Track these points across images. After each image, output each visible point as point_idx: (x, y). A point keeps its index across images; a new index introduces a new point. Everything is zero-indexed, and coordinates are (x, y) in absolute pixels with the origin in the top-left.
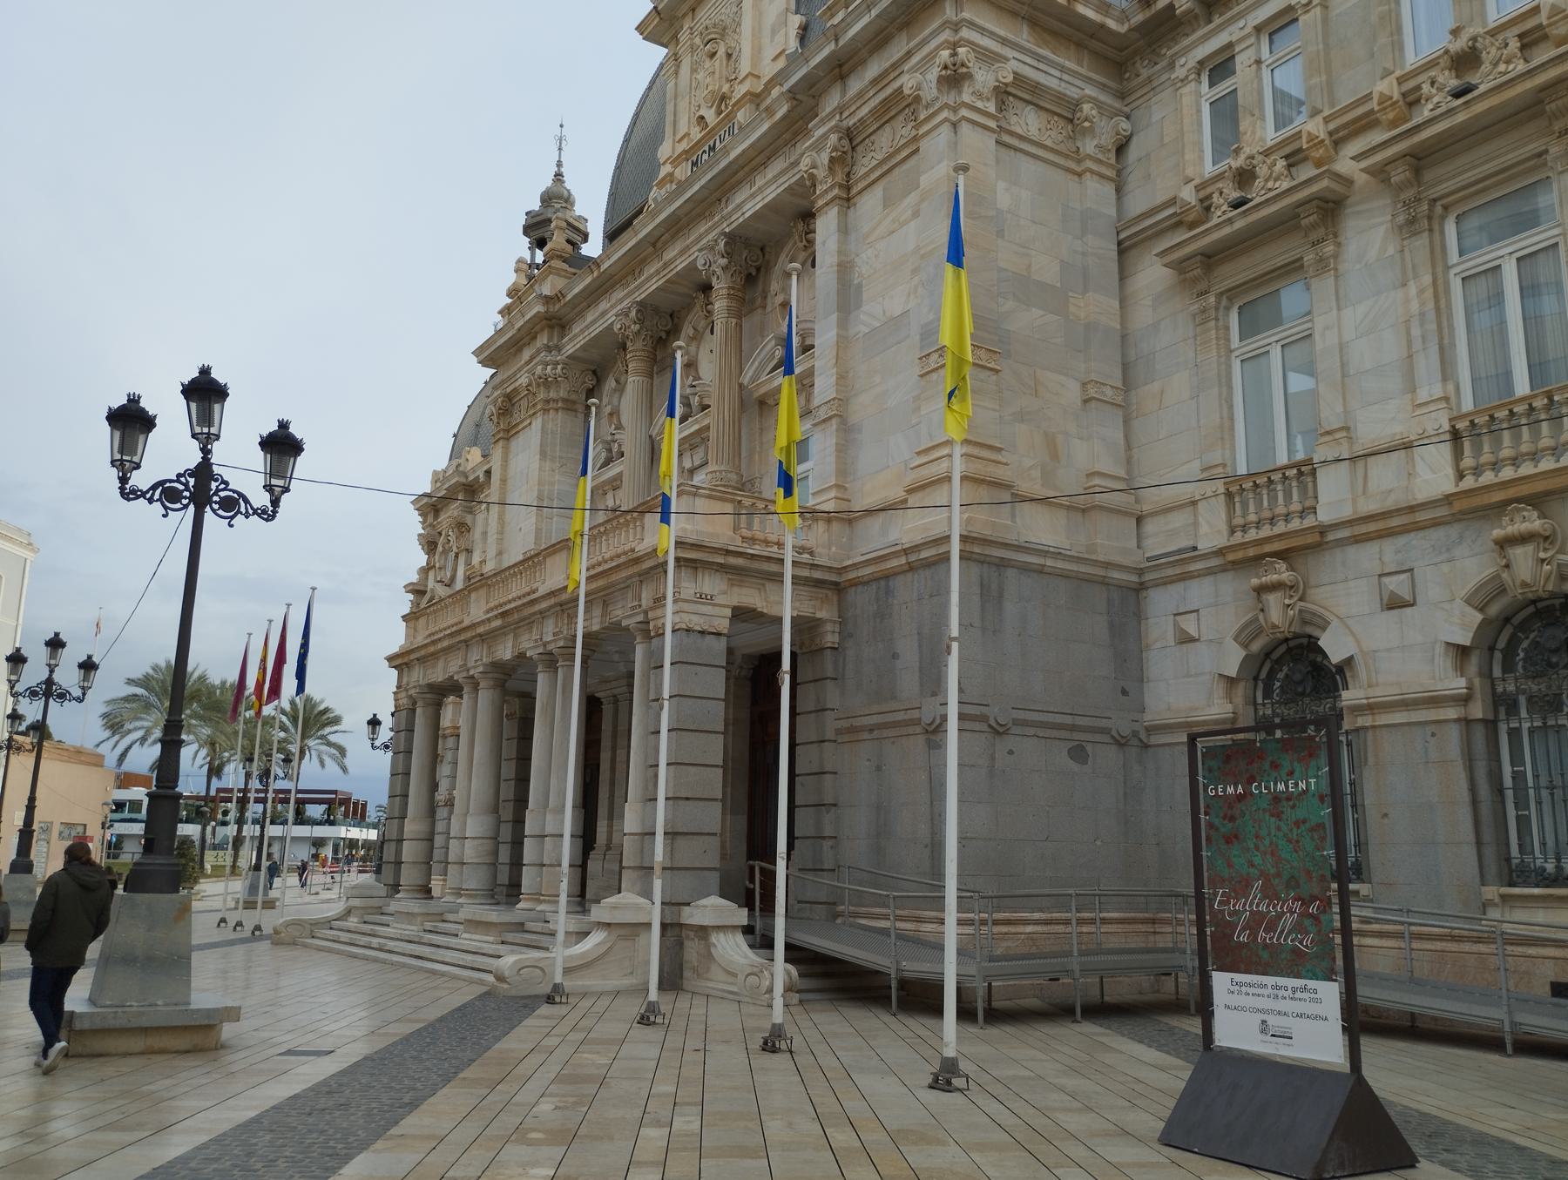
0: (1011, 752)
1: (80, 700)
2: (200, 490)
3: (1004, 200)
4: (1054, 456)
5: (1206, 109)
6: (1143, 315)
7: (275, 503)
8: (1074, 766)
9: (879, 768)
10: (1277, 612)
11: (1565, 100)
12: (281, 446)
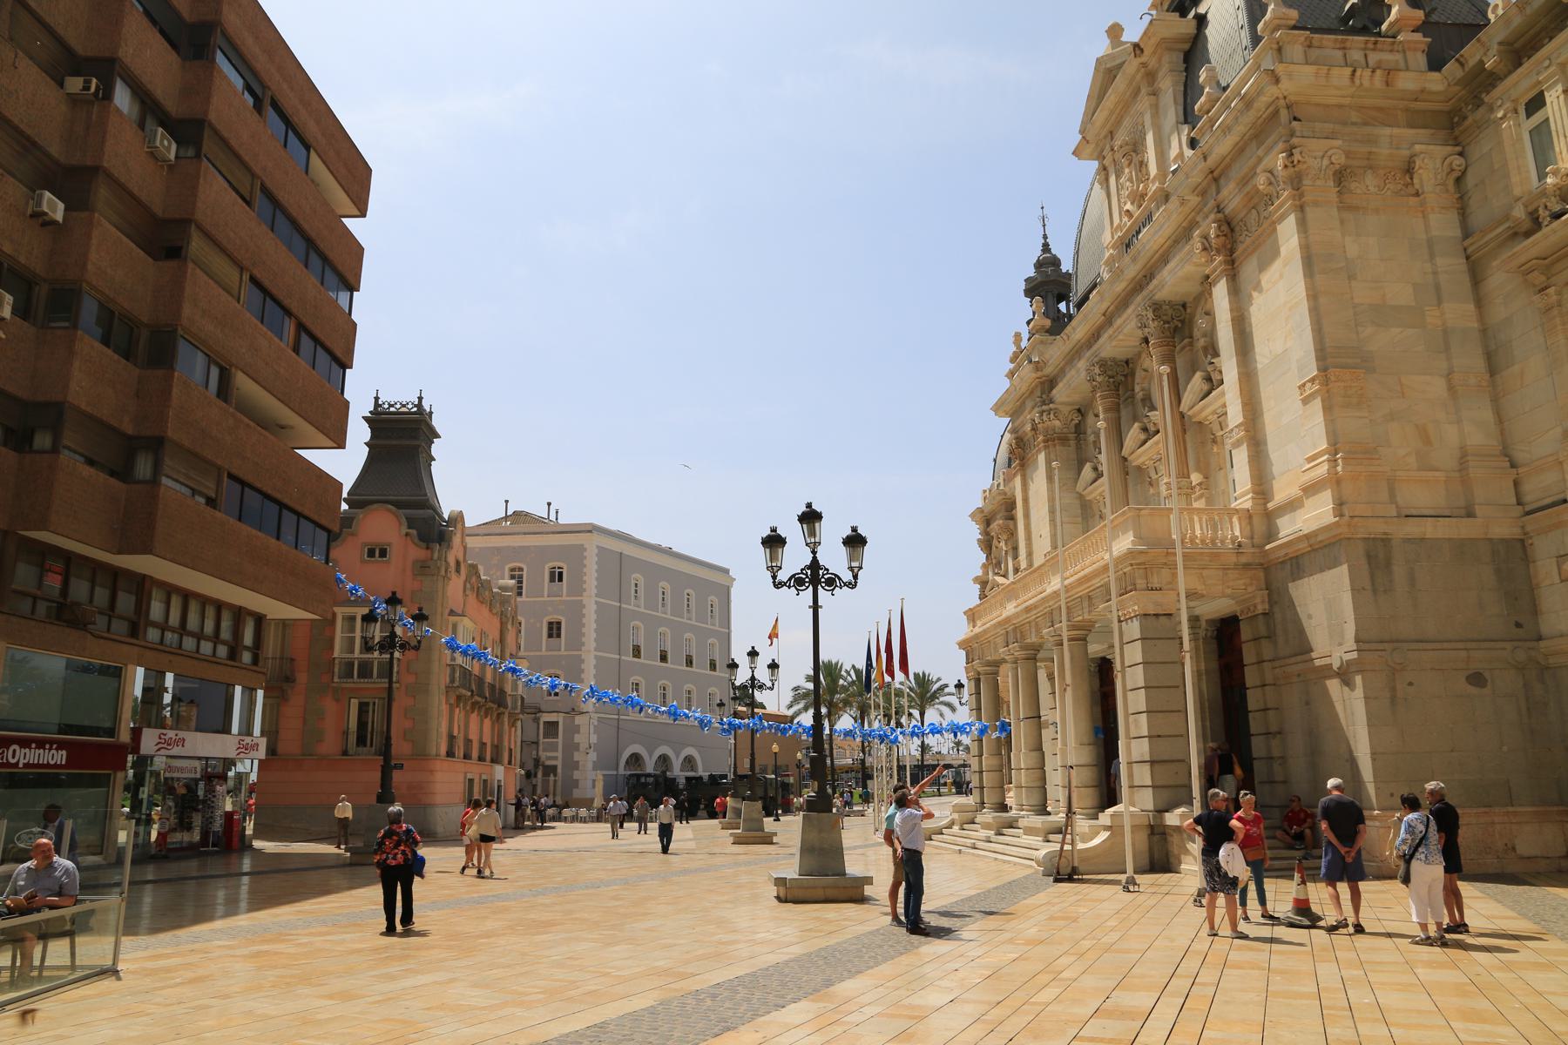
0: (1410, 684)
1: (771, 689)
2: (814, 577)
3: (1353, 250)
4: (1427, 441)
5: (1526, 137)
6: (1498, 312)
7: (856, 577)
8: (1473, 690)
9: (1307, 703)
12: (855, 541)
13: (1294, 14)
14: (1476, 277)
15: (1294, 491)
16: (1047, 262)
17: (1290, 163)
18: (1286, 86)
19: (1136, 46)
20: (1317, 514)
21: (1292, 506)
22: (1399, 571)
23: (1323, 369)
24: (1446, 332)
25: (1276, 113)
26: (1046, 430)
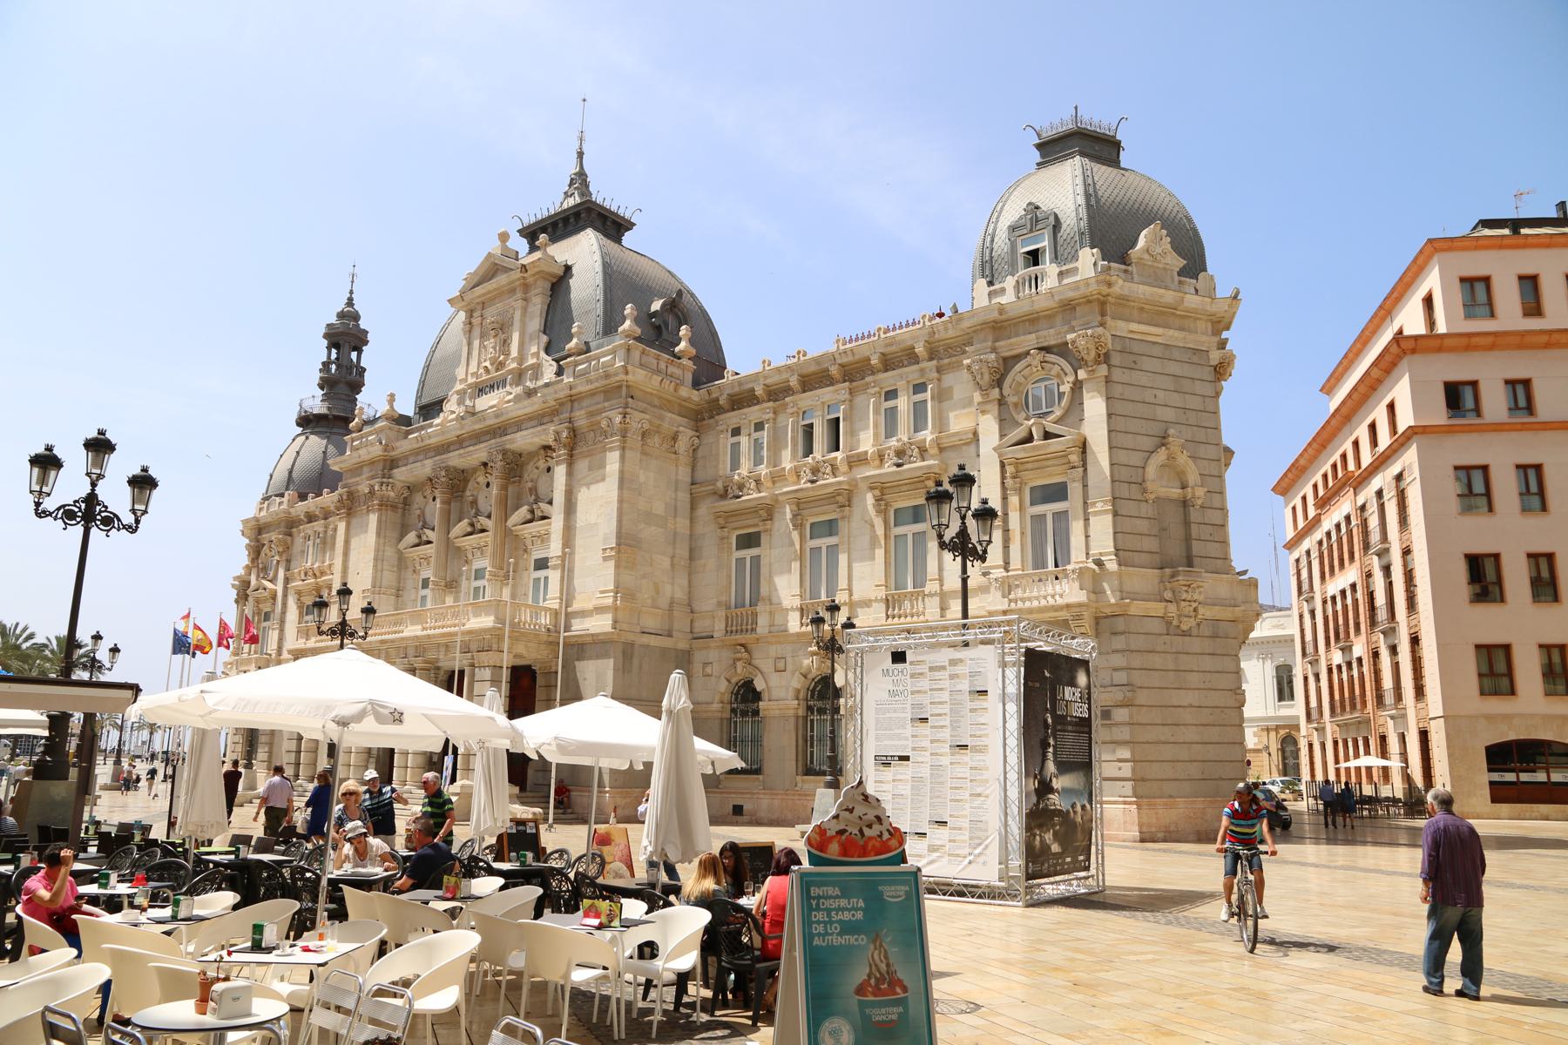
2: (89, 513)
4: (657, 592)
6: (699, 529)
7: (137, 521)
10: (741, 672)
11: (430, 1040)
12: (143, 483)
13: (639, 331)
14: (693, 508)
15: (589, 606)
16: (349, 315)
17: (623, 422)
18: (630, 377)
19: (524, 266)
20: (600, 624)
21: (583, 614)
22: (636, 661)
23: (619, 544)
24: (675, 533)
25: (620, 387)
26: (382, 497)
